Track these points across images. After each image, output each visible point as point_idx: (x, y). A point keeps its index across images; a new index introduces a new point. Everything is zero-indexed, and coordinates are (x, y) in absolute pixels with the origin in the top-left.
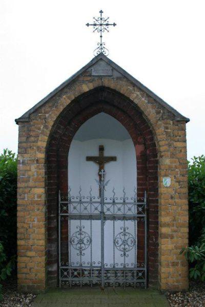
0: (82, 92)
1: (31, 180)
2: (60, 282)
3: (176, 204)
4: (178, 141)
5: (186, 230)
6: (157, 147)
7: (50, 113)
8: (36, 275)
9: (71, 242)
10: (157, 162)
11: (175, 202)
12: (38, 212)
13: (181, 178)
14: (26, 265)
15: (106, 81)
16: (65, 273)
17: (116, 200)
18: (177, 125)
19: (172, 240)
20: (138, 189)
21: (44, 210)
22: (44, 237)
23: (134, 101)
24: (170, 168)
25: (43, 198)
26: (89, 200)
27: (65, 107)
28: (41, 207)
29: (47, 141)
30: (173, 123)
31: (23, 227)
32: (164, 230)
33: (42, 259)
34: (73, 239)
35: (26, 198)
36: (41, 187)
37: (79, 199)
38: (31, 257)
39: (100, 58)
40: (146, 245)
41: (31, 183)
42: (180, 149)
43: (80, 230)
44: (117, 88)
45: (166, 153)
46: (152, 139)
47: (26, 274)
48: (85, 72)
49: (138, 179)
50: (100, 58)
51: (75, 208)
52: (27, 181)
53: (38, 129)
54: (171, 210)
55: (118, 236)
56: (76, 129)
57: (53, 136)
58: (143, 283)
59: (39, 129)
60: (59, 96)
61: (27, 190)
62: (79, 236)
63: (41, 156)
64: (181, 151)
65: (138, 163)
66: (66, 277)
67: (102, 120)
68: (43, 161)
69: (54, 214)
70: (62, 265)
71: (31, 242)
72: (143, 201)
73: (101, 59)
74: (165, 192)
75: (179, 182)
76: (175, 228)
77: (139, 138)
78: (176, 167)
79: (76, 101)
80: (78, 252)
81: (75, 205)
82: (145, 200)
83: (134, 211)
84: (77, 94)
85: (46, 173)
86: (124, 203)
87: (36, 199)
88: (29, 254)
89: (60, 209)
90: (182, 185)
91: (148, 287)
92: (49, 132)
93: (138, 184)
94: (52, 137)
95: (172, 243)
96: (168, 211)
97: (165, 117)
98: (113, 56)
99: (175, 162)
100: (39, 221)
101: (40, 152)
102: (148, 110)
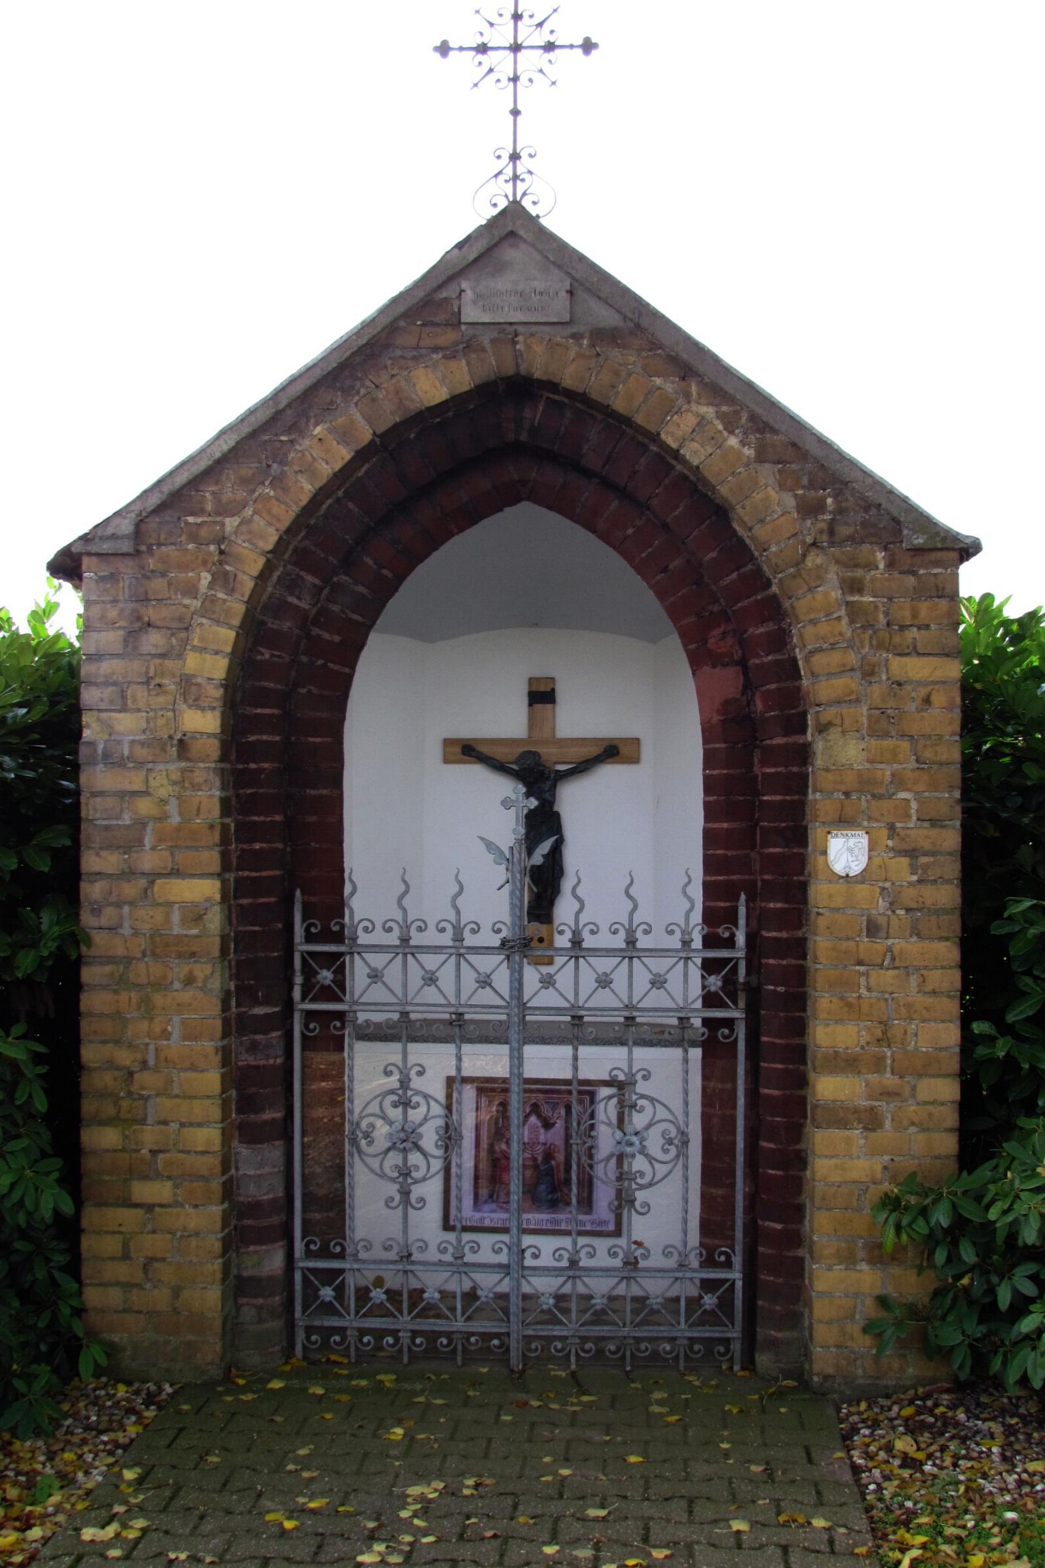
0: (415, 406)
1: (148, 841)
2: (300, 1336)
3: (894, 961)
4: (914, 651)
5: (948, 1090)
6: (805, 682)
7: (248, 512)
8: (176, 1292)
9: (354, 1142)
10: (804, 754)
11: (890, 949)
12: (187, 996)
13: (922, 836)
14: (126, 1245)
15: (539, 349)
16: (327, 1293)
17: (586, 934)
18: (913, 573)
19: (872, 1135)
20: (709, 889)
21: (216, 984)
22: (216, 1112)
23: (685, 452)
24: (866, 784)
25: (215, 921)
26: (446, 939)
27: (322, 481)
28: (202, 970)
29: (233, 653)
30: (891, 565)
31: (111, 1065)
32: (827, 1087)
33: (205, 1219)
34: (364, 1124)
35: (126, 924)
36: (203, 876)
37: (396, 932)
38: (150, 1208)
39: (511, 233)
40: (740, 1159)
41: (148, 860)
42: (923, 692)
43: (405, 1083)
44: (596, 384)
45: (846, 710)
46: (780, 640)
47: (127, 1286)
48: (422, 313)
49: (709, 838)
50: (511, 233)
51: (375, 976)
52: (130, 843)
53: (185, 593)
54: (869, 989)
55: (661, 1170)
56: (385, 590)
57: (262, 623)
58: (726, 1341)
59: (191, 590)
60: (293, 428)
61: (130, 890)
62: (396, 1114)
63: (204, 722)
64: (927, 701)
65: (709, 760)
66: (328, 1309)
67: (525, 535)
68: (213, 748)
69: (267, 1002)
70: (309, 1254)
71: (150, 1136)
72: (730, 943)
73: (512, 234)
74: (838, 902)
75: (912, 854)
76: (889, 1079)
77: (717, 632)
78: (898, 781)
79: (386, 447)
80: (393, 1190)
81: (377, 960)
82: (741, 938)
83: (686, 987)
84: (389, 418)
85: (225, 805)
86: (631, 950)
87: (177, 930)
88: (143, 1191)
89: (298, 980)
90: (925, 867)
91: (749, 1363)
92: (238, 609)
93: (709, 864)
94: (254, 630)
95: (873, 1153)
96: (852, 996)
97: (844, 531)
98: (577, 220)
99: (894, 756)
100: (189, 1035)
101: (197, 704)
102: (757, 497)
